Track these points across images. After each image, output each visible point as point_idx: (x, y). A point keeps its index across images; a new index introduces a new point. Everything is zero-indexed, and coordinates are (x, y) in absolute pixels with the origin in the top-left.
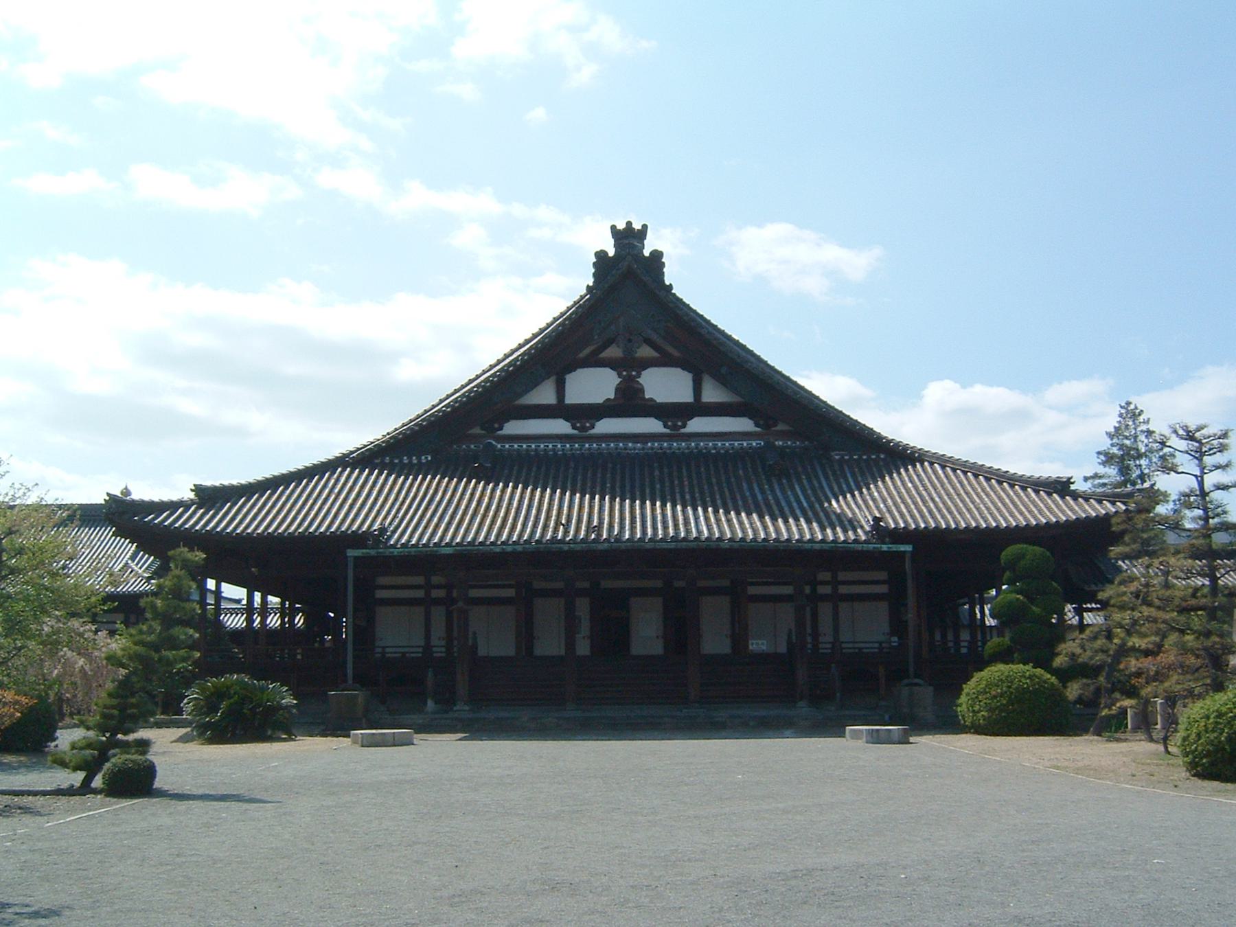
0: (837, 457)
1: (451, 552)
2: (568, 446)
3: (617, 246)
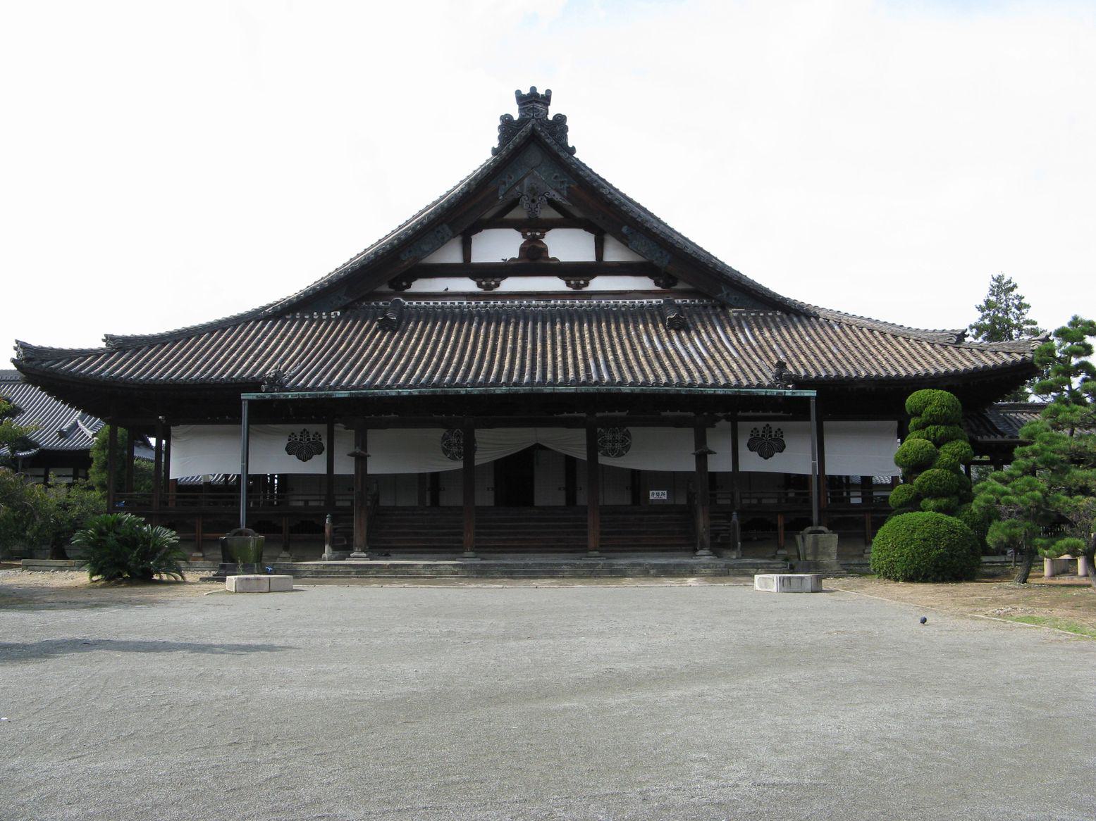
0: (735, 314)
1: (346, 396)
2: (473, 303)
3: (521, 110)
